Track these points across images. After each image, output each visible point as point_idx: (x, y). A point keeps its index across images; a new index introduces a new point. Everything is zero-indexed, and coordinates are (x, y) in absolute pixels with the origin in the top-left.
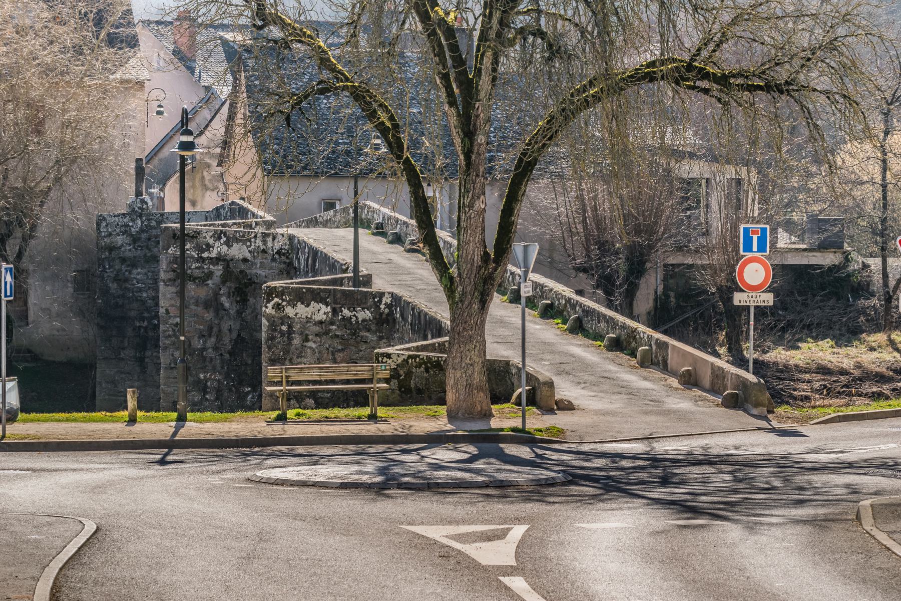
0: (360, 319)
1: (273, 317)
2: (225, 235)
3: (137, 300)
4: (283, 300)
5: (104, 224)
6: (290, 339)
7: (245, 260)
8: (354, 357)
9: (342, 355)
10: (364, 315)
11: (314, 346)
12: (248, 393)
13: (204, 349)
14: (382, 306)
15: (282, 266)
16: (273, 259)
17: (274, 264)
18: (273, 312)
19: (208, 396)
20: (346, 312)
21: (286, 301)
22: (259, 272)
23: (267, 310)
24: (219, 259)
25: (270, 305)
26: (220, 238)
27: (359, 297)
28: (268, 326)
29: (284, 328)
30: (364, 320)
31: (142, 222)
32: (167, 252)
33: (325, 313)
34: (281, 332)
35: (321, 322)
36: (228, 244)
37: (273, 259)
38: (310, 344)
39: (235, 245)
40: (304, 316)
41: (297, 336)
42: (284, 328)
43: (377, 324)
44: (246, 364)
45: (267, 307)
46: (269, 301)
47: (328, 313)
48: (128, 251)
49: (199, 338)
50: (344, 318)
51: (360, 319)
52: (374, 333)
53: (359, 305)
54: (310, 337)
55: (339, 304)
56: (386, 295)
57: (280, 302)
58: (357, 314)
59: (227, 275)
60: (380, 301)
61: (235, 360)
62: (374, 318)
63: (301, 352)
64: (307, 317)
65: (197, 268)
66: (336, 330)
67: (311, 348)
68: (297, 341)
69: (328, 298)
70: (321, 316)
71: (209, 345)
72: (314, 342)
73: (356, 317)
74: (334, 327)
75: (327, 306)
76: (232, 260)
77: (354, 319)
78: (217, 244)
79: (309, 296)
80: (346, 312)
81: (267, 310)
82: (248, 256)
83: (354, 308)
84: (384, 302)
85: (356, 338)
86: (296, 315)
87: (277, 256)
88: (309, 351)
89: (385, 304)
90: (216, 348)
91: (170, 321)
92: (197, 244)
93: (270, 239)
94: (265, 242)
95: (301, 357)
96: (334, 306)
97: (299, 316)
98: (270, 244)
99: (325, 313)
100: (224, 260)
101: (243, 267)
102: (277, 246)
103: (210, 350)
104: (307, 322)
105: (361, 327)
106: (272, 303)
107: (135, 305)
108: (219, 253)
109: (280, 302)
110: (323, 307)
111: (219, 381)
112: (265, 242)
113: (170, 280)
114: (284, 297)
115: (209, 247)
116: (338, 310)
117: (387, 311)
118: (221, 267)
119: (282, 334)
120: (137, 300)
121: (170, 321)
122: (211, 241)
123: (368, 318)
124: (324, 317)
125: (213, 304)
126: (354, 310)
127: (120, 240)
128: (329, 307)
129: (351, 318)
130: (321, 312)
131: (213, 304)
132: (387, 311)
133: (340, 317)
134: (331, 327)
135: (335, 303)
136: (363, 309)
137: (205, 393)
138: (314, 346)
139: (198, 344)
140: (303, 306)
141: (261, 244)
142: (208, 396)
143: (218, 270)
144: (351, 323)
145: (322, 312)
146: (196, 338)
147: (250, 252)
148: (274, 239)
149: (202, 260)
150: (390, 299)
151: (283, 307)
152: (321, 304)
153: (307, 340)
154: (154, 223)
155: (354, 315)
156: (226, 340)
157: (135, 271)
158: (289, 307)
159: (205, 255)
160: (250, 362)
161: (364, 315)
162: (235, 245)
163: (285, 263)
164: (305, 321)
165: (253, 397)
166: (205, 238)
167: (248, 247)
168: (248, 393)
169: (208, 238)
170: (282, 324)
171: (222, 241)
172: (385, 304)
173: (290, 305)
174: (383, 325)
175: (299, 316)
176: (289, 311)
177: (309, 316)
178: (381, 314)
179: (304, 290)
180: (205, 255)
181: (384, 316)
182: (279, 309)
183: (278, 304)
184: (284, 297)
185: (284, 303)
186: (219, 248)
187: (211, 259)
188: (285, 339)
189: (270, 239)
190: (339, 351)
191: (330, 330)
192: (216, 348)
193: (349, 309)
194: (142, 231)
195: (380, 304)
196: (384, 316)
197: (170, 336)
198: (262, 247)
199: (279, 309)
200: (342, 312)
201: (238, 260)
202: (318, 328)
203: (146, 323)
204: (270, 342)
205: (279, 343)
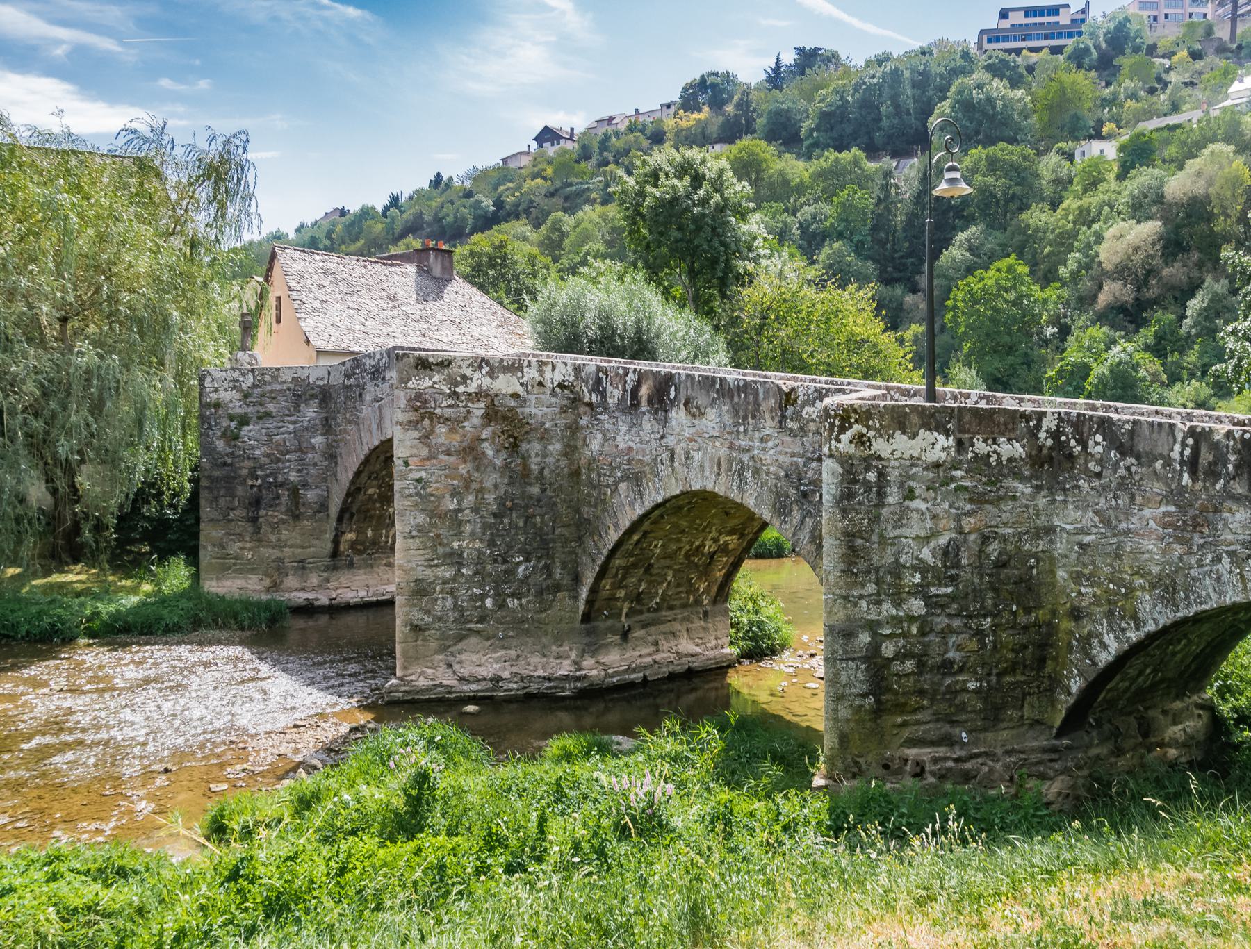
0: (1005, 458)
1: (850, 458)
2: (488, 363)
3: (249, 458)
4: (869, 428)
5: (208, 380)
6: (881, 494)
7: (515, 396)
8: (993, 523)
9: (973, 521)
10: (1011, 449)
11: (923, 506)
12: (519, 564)
13: (459, 510)
14: (1042, 435)
15: (565, 402)
16: (553, 394)
17: (554, 400)
18: (852, 449)
19: (464, 571)
20: (980, 446)
21: (875, 429)
22: (534, 411)
23: (840, 446)
24: (480, 394)
25: (845, 437)
26: (480, 367)
27: (1002, 421)
28: (842, 475)
29: (871, 476)
30: (1010, 460)
31: (254, 377)
32: (406, 388)
33: (944, 449)
34: (866, 483)
35: (937, 465)
36: (491, 374)
37: (553, 394)
38: (916, 504)
39: (501, 376)
40: (906, 455)
41: (894, 489)
42: (871, 476)
43: (1032, 466)
44: (517, 528)
45: (839, 441)
46: (843, 430)
47: (949, 448)
48: (238, 408)
49: (452, 495)
50: (977, 457)
51: (1005, 458)
52: (1028, 479)
53: (1002, 434)
54: (917, 492)
55: (968, 432)
56: (1049, 416)
57: (864, 430)
58: (999, 450)
59: (491, 415)
60: (1038, 427)
61: (502, 522)
62: (1029, 456)
63: (901, 518)
64: (912, 457)
65: (449, 406)
66: (963, 477)
67: (917, 510)
68: (893, 497)
69: (949, 422)
70: (937, 455)
71: (465, 504)
72: (924, 499)
73: (998, 454)
74: (959, 473)
75: (948, 436)
76: (497, 395)
77: (994, 457)
78: (477, 375)
79: (915, 419)
80: (980, 446)
81: (840, 446)
82: (520, 390)
83: (994, 439)
84: (1044, 428)
85: (998, 489)
86: (892, 454)
87: (558, 390)
88: (915, 516)
89: (1047, 432)
90: (475, 510)
91: (411, 476)
92: (449, 376)
93: (548, 369)
94: (541, 372)
95: (902, 526)
96: (960, 436)
97: (898, 454)
98: (548, 375)
99: (944, 449)
100: (487, 395)
101: (512, 403)
102: (558, 378)
103: (467, 512)
104: (913, 465)
105: (1005, 471)
106: (849, 434)
107: (247, 463)
108: (480, 386)
109: (864, 430)
110: (941, 439)
111: (479, 551)
112: (541, 372)
113: (410, 422)
114: (871, 423)
115: (465, 378)
116: (967, 444)
117: (1049, 442)
118: (482, 405)
119: (867, 485)
120: (249, 458)
121: (411, 476)
122: (468, 372)
123: (1017, 456)
124: (943, 455)
125: (471, 451)
126: (995, 443)
127: (227, 396)
128: (951, 439)
129: (989, 456)
130: (938, 446)
131: (471, 451)
132: (1049, 442)
133: (970, 455)
134: (954, 473)
135: (960, 432)
136: (1009, 440)
137: (460, 565)
138: (923, 506)
139: (450, 504)
140: (905, 437)
141: (536, 375)
142: (464, 571)
143: (478, 409)
144: (988, 464)
145: (938, 447)
146: (447, 496)
147: (522, 384)
148: (554, 368)
149: (454, 395)
150: (1055, 423)
151: (869, 440)
152: (936, 434)
153: (910, 495)
154: (268, 378)
155: (995, 452)
156: (490, 498)
157: (246, 428)
158: (880, 440)
159: (461, 389)
160: (521, 524)
161: (1011, 449)
162: (501, 376)
163: (568, 398)
164: (908, 463)
165: (527, 569)
166: (460, 367)
167: (518, 379)
168: (519, 564)
169: (464, 366)
170: (867, 469)
171: (484, 371)
172: (1047, 432)
173: (881, 436)
174: (1042, 466)
175: (898, 454)
176: (880, 446)
177: (916, 455)
178: (1040, 448)
179: (907, 410)
180: (461, 389)
181: (1045, 451)
182: (863, 443)
183: (861, 435)
184: (871, 423)
185: (871, 433)
186: (479, 380)
187: (470, 394)
188: (873, 496)
189: (548, 369)
190: (968, 514)
191: (953, 479)
192: (475, 510)
193: (985, 441)
194: (254, 386)
195: (1039, 431)
196: (1045, 451)
197: (410, 495)
198: (539, 379)
199: (863, 443)
200: (973, 445)
201: (505, 395)
202: (931, 475)
203: (259, 482)
204: (845, 503)
205: (860, 504)
